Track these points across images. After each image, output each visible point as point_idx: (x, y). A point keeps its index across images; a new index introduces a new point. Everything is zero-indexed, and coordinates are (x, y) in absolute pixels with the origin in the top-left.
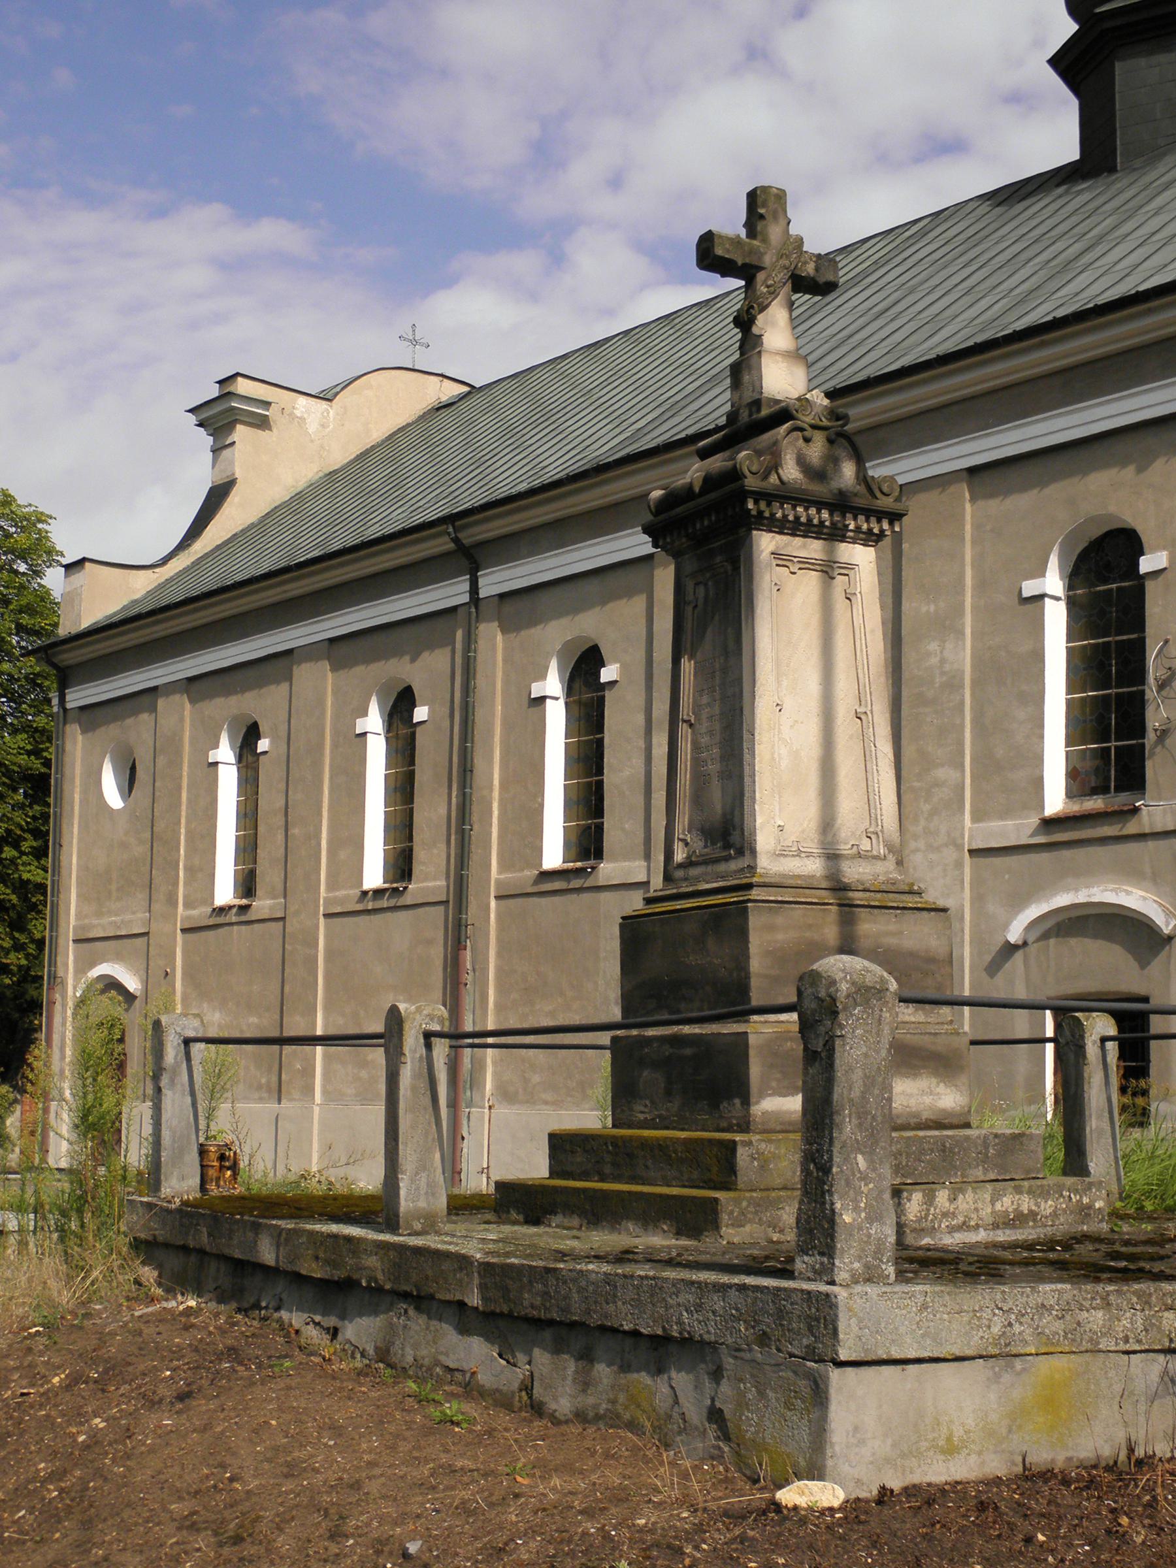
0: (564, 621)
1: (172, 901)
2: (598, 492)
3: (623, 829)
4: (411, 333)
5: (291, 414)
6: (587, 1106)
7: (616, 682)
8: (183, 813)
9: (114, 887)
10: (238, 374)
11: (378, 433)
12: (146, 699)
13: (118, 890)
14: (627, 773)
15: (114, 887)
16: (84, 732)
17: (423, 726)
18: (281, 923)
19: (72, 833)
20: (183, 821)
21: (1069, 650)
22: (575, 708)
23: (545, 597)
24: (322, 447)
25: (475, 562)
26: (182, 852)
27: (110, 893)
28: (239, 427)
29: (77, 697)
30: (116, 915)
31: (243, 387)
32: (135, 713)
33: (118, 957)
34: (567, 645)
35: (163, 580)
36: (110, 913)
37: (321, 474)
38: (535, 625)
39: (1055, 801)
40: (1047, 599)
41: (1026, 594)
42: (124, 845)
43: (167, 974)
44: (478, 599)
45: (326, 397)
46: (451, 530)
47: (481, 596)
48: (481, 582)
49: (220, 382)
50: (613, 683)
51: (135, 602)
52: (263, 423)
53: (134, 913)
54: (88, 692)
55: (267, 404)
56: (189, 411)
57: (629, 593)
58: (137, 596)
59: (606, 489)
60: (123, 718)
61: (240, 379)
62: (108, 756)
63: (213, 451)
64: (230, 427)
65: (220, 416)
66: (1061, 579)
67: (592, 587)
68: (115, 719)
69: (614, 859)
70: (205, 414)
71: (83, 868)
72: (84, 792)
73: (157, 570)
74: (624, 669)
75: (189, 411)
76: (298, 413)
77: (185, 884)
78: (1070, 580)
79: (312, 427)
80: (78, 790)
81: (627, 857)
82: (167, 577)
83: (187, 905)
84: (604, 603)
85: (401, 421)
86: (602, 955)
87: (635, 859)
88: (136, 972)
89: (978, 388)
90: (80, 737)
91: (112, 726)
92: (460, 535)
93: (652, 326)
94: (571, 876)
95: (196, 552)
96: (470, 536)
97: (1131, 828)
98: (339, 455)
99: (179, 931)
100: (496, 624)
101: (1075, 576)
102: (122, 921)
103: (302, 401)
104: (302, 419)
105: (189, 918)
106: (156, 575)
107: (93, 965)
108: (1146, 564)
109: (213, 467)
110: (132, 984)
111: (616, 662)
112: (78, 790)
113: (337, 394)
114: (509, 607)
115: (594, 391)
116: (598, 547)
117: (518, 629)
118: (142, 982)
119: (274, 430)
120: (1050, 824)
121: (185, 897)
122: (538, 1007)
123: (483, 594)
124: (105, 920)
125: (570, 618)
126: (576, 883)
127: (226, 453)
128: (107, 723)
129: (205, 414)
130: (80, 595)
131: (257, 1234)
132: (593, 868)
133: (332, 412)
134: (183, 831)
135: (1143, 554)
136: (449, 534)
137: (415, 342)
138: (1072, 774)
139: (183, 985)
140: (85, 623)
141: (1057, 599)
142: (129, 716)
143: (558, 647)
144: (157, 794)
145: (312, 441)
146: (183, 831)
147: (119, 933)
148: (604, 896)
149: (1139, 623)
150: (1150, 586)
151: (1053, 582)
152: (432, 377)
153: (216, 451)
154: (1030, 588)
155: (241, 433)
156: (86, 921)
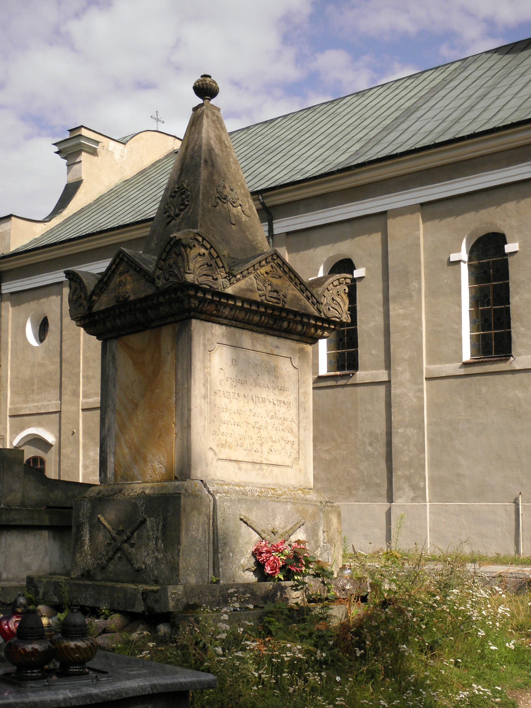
0: (329, 247)
1: (76, 394)
2: (353, 179)
3: (371, 354)
4: (156, 115)
5: (107, 149)
6: (352, 500)
7: (364, 277)
8: (81, 348)
9: (36, 387)
10: (82, 126)
11: (148, 162)
12: (55, 288)
13: (38, 388)
14: (372, 324)
15: (36, 387)
16: (13, 306)
17: (515, 256)
18: (58, 414)
19: (8, 359)
20: (81, 352)
21: (470, 288)
22: (473, 269)
23: (315, 235)
24: (121, 167)
25: (271, 216)
26: (81, 368)
27: (33, 391)
28: (83, 154)
29: (8, 287)
30: (37, 402)
31: (84, 132)
32: (48, 296)
33: (39, 424)
34: (329, 259)
35: (49, 229)
36: (33, 401)
37: (121, 181)
38: (310, 248)
39: (467, 356)
40: (462, 263)
41: (451, 260)
42: (41, 365)
43: (74, 433)
44: (273, 235)
45: (123, 142)
46: (260, 198)
47: (275, 233)
48: (275, 226)
49: (70, 131)
50: (361, 278)
51: (36, 240)
52: (94, 152)
53: (49, 401)
54: (34, 281)
55: (97, 143)
56: (54, 144)
57: (370, 232)
58: (37, 236)
59: (359, 177)
60: (39, 298)
61: (83, 129)
62: (29, 318)
63: (68, 166)
64: (78, 153)
65: (72, 147)
66: (467, 253)
67: (347, 228)
68: (33, 299)
69: (365, 369)
70: (63, 146)
71: (15, 378)
72: (14, 337)
73: (46, 224)
74: (368, 270)
75: (54, 144)
76: (110, 149)
77: (83, 385)
78: (470, 253)
79: (117, 156)
80: (10, 336)
81: (374, 367)
82: (51, 227)
83: (85, 397)
84: (353, 237)
85: (157, 158)
86: (360, 419)
87: (379, 369)
88: (52, 432)
89: (512, 144)
90: (11, 309)
91: (31, 303)
92: (265, 201)
93: (279, 120)
94: (339, 378)
95: (64, 216)
96: (271, 201)
97: (351, 381)
98: (130, 173)
99: (80, 410)
100: (285, 248)
101: (471, 252)
102: (42, 405)
103: (112, 143)
104: (112, 152)
105: (87, 403)
106: (46, 226)
107: (23, 429)
108: (509, 248)
109: (68, 174)
110: (51, 438)
111: (363, 267)
112: (10, 336)
113: (128, 141)
114: (292, 239)
115: (294, 139)
116: (351, 207)
117: (298, 251)
118: (56, 438)
119: (100, 156)
120: (466, 365)
121: (83, 392)
122: (319, 448)
123: (276, 232)
124: (30, 405)
125: (331, 245)
126: (342, 382)
127: (76, 167)
128: (28, 301)
129: (63, 146)
130: (10, 234)
131: (253, 571)
132: (353, 374)
133: (126, 150)
134: (81, 357)
135: (506, 243)
136: (259, 200)
137: (158, 120)
138: (329, 363)
139: (83, 439)
140: (13, 248)
141: (465, 262)
142: (43, 298)
143: (325, 259)
144: (64, 338)
145: (117, 164)
146: (81, 357)
147: (40, 412)
148: (359, 389)
149: (506, 275)
150: (510, 259)
151: (463, 255)
152: (170, 137)
153: (69, 166)
154: (454, 257)
155: (84, 156)
156: (18, 406)
